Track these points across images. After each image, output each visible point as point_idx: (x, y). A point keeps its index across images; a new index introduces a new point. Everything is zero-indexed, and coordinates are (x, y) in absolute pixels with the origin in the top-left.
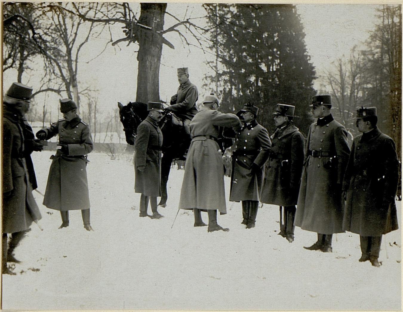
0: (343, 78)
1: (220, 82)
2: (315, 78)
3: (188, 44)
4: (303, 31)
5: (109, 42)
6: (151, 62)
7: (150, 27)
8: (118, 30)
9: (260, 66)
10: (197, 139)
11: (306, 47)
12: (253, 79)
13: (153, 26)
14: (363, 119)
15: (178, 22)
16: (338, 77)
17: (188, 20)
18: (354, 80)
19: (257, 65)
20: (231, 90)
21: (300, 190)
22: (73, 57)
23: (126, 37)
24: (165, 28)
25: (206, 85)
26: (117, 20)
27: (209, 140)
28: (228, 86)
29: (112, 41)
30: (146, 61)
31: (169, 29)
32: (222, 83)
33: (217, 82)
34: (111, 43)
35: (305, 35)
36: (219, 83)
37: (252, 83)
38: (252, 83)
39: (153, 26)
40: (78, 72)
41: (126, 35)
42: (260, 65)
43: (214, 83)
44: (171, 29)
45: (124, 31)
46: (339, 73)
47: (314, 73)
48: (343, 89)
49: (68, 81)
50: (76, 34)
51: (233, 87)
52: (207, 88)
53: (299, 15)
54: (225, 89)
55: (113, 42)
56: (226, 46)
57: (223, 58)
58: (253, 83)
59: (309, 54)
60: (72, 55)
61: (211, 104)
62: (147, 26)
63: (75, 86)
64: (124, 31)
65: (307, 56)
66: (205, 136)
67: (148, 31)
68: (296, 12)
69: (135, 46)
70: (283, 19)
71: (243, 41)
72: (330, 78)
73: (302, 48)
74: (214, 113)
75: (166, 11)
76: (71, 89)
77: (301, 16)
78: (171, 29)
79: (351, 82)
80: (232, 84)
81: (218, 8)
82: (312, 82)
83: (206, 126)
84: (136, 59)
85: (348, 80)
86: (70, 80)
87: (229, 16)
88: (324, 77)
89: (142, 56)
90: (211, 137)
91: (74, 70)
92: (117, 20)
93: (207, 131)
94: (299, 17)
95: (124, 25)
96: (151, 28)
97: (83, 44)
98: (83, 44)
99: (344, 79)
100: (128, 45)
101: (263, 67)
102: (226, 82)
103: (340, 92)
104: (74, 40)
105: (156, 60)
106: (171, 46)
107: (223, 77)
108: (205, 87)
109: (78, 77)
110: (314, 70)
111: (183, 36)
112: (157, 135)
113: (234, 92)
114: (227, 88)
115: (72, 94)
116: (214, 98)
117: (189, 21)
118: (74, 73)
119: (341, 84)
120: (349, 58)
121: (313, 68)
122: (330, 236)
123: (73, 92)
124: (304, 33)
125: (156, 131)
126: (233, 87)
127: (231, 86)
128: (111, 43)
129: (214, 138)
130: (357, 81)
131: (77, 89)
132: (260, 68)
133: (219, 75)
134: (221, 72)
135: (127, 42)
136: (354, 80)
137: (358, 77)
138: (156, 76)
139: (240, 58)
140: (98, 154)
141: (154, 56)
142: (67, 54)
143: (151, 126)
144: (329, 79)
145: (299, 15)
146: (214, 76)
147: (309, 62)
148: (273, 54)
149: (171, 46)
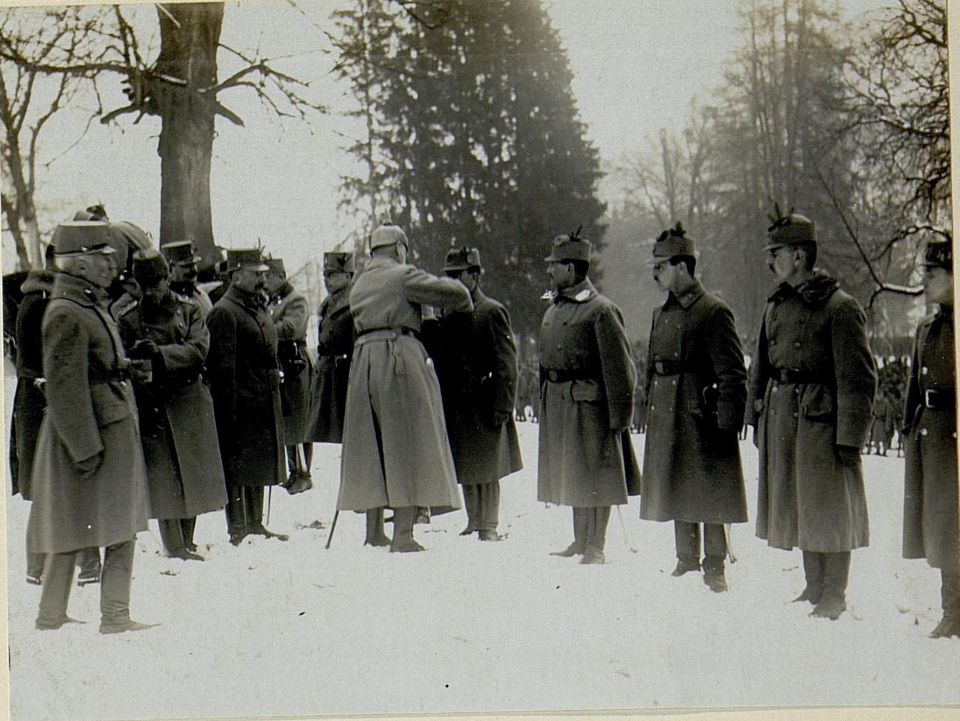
0: (670, 171)
1: (382, 192)
2: (600, 175)
3: (280, 114)
4: (568, 67)
5: (93, 116)
6: (189, 160)
7: (183, 79)
8: (113, 89)
9: (473, 152)
10: (374, 338)
11: (576, 106)
12: (455, 184)
13: (190, 76)
14: (670, 260)
15: (248, 65)
16: (659, 170)
17: (262, 61)
18: (696, 174)
19: (461, 149)
20: (407, 210)
21: (798, 488)
22: (24, 151)
23: (129, 103)
24: (221, 79)
25: (348, 202)
26: (108, 66)
27: (403, 338)
28: (400, 202)
29: (100, 112)
30: (178, 157)
31: (225, 82)
32: (385, 195)
33: (374, 193)
34: (99, 117)
35: (572, 76)
36: (377, 196)
37: (452, 193)
38: (452, 193)
39: (190, 76)
40: (36, 185)
41: (131, 97)
42: (473, 148)
43: (367, 198)
44: (232, 82)
45: (126, 91)
46: (660, 160)
47: (595, 163)
48: (670, 195)
49: (14, 207)
50: (28, 95)
51: (413, 203)
52: (350, 208)
53: (557, 31)
54: (393, 209)
55: (104, 115)
56: (391, 109)
57: (386, 138)
58: (458, 193)
59: (583, 120)
60: (20, 145)
61: (393, 248)
62: (174, 76)
63: (30, 218)
64: (126, 91)
65: (579, 124)
66: (389, 328)
67: (179, 89)
68: (548, 25)
69: (154, 124)
70: (518, 41)
71: (430, 94)
72: (640, 171)
73: (567, 106)
74: (408, 273)
75: (220, 42)
76: (22, 225)
77: (560, 33)
78: (232, 82)
79: (690, 180)
80: (409, 195)
81: (366, 23)
82: (595, 184)
83: (391, 307)
84: (157, 154)
85: (685, 175)
86: (18, 205)
87: (394, 40)
88: (627, 170)
89: (167, 147)
90: (405, 331)
91: (27, 180)
92: (108, 66)
93: (395, 316)
94: (556, 36)
95: (126, 77)
96: (184, 82)
97: (46, 117)
98: (46, 117)
99: (674, 174)
100: (137, 122)
101: (479, 153)
102: (394, 192)
103: (666, 203)
104: (23, 111)
105: (200, 154)
106: (237, 121)
107: (387, 182)
108: (344, 205)
109: (38, 197)
110: (596, 157)
111: (267, 97)
112: (258, 329)
113: (415, 215)
114: (398, 206)
115: (23, 235)
116: (397, 233)
117: (266, 64)
118: (28, 189)
119: (667, 185)
120: (682, 127)
121: (596, 151)
122: (311, 444)
123: (26, 232)
124: (569, 72)
125: (253, 320)
126: (413, 203)
127: (408, 201)
128: (99, 117)
129: (414, 331)
130: (706, 177)
131: (37, 225)
132: (474, 157)
133: (377, 179)
134: (381, 170)
135: (138, 113)
136: (696, 174)
137: (706, 169)
138: (203, 192)
139: (424, 135)
140: (606, 542)
141: (195, 145)
142: (8, 144)
143: (239, 310)
144: (640, 175)
145: (557, 31)
146: (365, 181)
147: (583, 138)
148: (499, 123)
149: (237, 121)
